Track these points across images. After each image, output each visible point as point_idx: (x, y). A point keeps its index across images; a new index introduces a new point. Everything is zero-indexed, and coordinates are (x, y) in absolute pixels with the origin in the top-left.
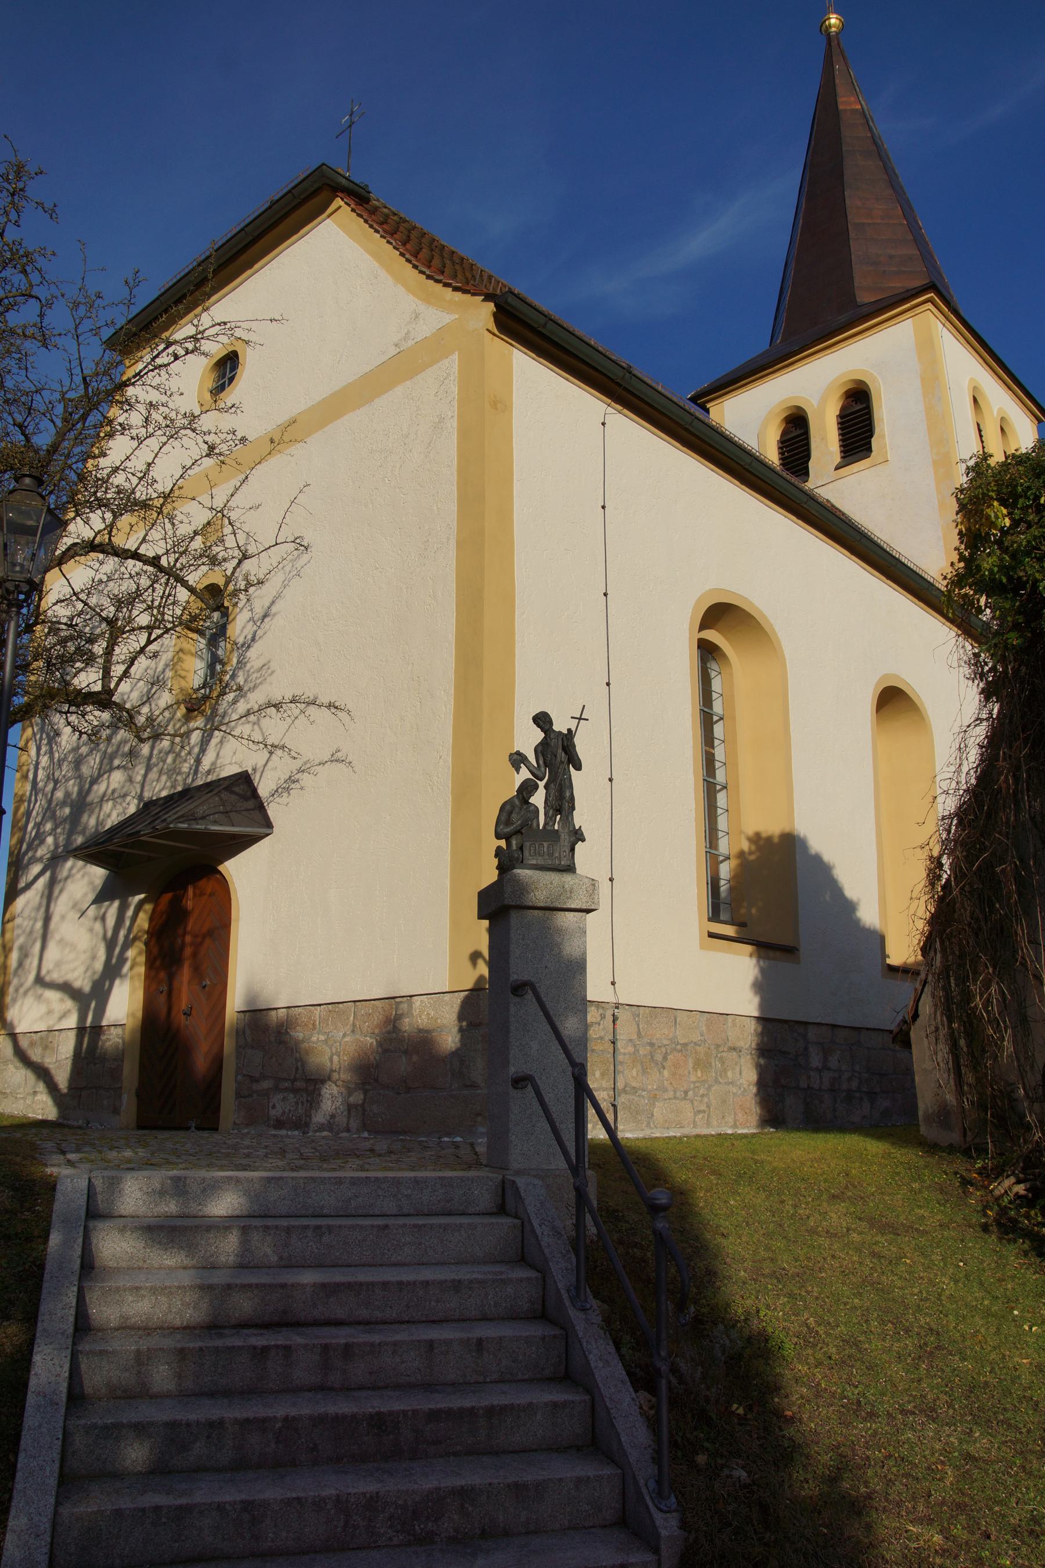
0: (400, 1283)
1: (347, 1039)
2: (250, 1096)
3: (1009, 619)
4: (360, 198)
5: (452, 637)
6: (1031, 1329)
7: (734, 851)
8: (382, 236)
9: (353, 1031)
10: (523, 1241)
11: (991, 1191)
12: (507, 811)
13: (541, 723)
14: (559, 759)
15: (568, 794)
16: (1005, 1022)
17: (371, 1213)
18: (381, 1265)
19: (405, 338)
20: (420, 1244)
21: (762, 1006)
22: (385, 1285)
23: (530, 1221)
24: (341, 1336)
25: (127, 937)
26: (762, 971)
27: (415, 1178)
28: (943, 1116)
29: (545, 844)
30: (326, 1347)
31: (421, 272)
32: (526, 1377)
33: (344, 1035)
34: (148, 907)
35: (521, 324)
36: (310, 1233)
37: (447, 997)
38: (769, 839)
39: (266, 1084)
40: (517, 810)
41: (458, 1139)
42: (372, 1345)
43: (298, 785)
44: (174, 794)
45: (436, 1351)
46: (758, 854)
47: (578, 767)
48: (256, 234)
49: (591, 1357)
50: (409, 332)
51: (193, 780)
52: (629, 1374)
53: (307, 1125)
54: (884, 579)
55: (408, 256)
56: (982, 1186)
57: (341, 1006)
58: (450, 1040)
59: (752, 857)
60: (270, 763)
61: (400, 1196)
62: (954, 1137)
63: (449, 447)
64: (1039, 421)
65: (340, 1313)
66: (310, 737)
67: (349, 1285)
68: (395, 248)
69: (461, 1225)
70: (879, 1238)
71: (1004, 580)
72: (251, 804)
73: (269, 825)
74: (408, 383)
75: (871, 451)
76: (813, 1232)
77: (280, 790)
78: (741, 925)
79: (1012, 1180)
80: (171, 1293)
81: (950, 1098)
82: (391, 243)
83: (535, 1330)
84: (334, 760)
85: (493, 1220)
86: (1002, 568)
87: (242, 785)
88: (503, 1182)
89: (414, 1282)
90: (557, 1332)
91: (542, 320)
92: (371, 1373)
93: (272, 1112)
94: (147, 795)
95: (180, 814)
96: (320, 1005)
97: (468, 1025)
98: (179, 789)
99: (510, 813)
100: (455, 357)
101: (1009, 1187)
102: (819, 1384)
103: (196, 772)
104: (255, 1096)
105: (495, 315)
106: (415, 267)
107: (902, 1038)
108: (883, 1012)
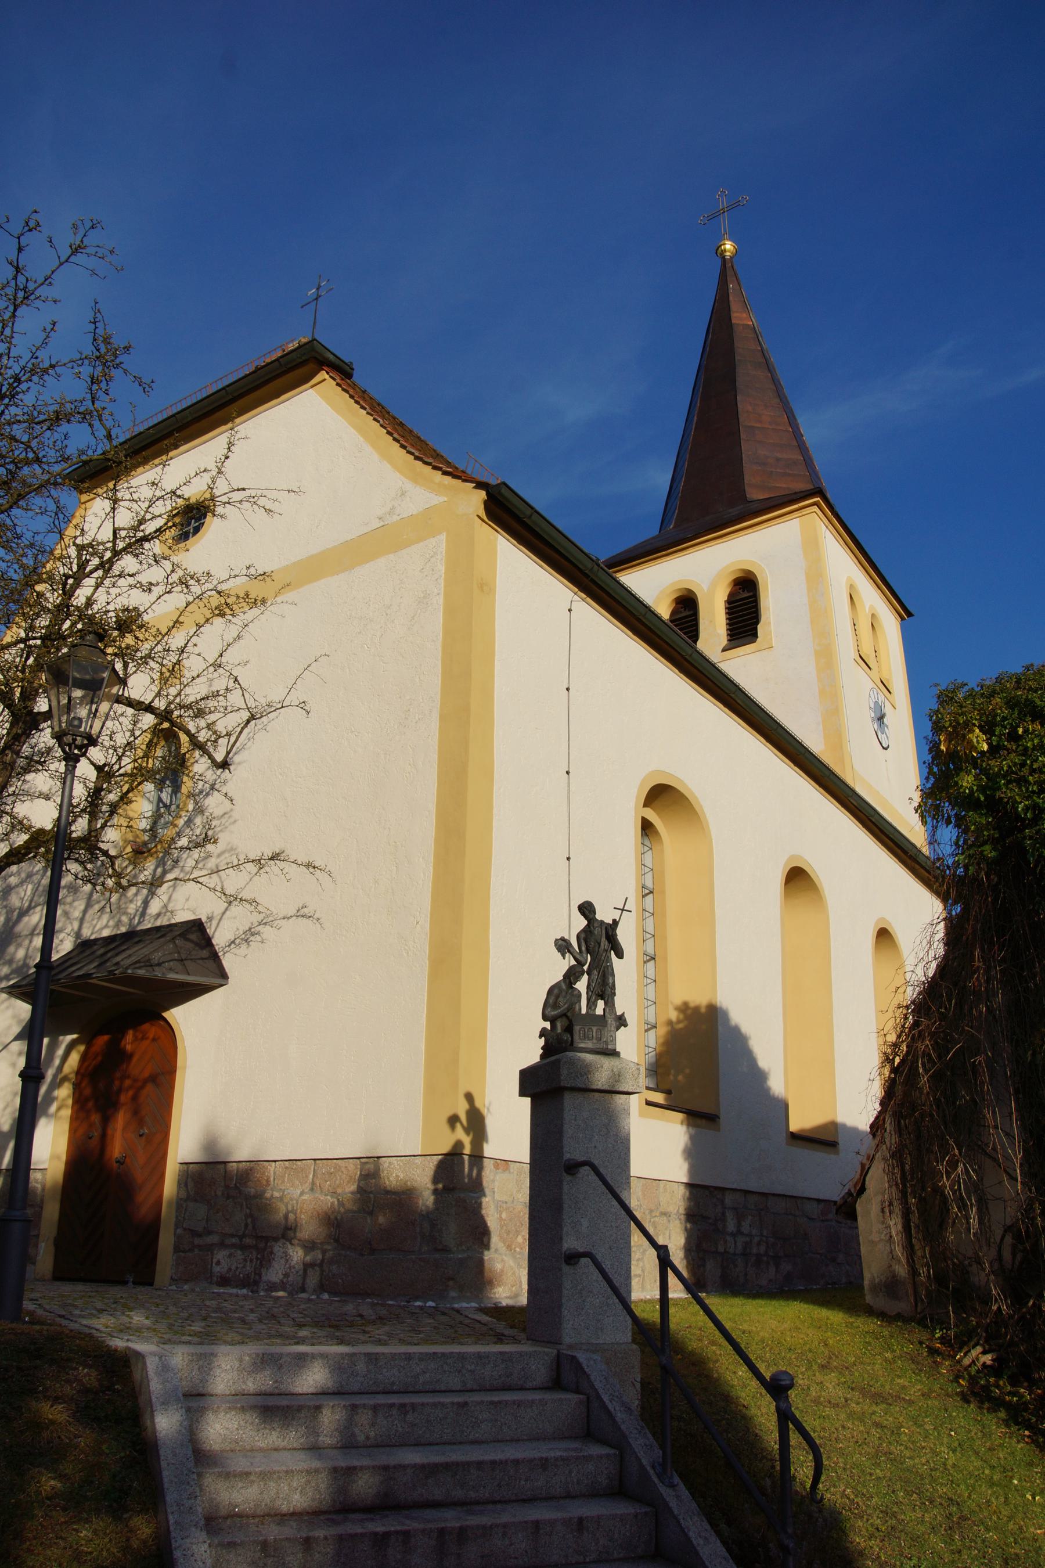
0: (493, 1463)
1: (305, 1197)
2: (191, 1250)
3: (985, 833)
4: (343, 372)
5: (432, 806)
6: (1034, 1498)
7: (662, 1020)
8: (368, 413)
9: (312, 1189)
10: (588, 1416)
11: (959, 1361)
12: (554, 993)
13: (587, 912)
14: (602, 947)
15: (611, 981)
16: (970, 1201)
17: (438, 1388)
18: (460, 1443)
19: (392, 511)
20: (496, 1420)
21: (692, 1171)
22: (479, 1464)
23: (598, 1397)
24: (451, 1519)
25: (55, 1076)
26: (692, 1138)
27: (479, 1353)
28: (891, 1286)
29: (594, 1029)
30: (442, 1532)
31: (409, 452)
32: (621, 1555)
33: (302, 1193)
34: (82, 1048)
35: (507, 512)
36: (394, 1412)
37: (418, 1160)
38: (697, 1009)
39: (214, 1239)
40: (564, 993)
41: (430, 1304)
42: (484, 1527)
43: (258, 938)
44: (116, 935)
45: (541, 1531)
46: (686, 1023)
47: (620, 955)
48: (235, 394)
49: (691, 1534)
50: (394, 507)
51: (139, 923)
52: (729, 1550)
53: (256, 1283)
54: (792, 765)
55: (395, 435)
56: (949, 1356)
57: (299, 1163)
58: (427, 1199)
59: (681, 1026)
60: (228, 913)
61: (464, 1371)
62: (903, 1306)
63: (435, 622)
64: (902, 619)
65: (438, 1494)
66: (274, 891)
67: (447, 1466)
68: (381, 426)
69: (533, 1402)
70: (874, 1408)
71: (982, 799)
72: (205, 953)
73: (224, 976)
74: (391, 556)
75: (757, 637)
76: (817, 1402)
77: (237, 941)
78: (668, 1092)
79: (979, 1349)
80: (280, 1478)
81: (902, 1270)
82: (378, 422)
83: (623, 1509)
84: (301, 914)
85: (548, 1396)
86: (982, 789)
87: (195, 934)
88: (558, 1355)
89: (506, 1461)
90: (648, 1509)
91: (529, 512)
92: (482, 1557)
93: (217, 1269)
94: (87, 933)
95: (134, 959)
96: (275, 1161)
97: (444, 1187)
98: (123, 930)
99: (557, 997)
100: (443, 537)
101: (979, 1357)
102: (879, 1557)
103: (143, 914)
104: (196, 1251)
105: (486, 503)
106: (403, 447)
107: (846, 1209)
108: (825, 1180)
